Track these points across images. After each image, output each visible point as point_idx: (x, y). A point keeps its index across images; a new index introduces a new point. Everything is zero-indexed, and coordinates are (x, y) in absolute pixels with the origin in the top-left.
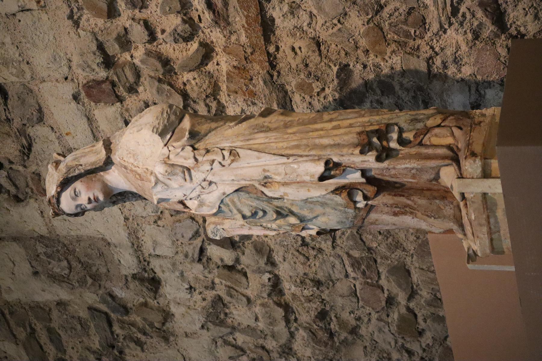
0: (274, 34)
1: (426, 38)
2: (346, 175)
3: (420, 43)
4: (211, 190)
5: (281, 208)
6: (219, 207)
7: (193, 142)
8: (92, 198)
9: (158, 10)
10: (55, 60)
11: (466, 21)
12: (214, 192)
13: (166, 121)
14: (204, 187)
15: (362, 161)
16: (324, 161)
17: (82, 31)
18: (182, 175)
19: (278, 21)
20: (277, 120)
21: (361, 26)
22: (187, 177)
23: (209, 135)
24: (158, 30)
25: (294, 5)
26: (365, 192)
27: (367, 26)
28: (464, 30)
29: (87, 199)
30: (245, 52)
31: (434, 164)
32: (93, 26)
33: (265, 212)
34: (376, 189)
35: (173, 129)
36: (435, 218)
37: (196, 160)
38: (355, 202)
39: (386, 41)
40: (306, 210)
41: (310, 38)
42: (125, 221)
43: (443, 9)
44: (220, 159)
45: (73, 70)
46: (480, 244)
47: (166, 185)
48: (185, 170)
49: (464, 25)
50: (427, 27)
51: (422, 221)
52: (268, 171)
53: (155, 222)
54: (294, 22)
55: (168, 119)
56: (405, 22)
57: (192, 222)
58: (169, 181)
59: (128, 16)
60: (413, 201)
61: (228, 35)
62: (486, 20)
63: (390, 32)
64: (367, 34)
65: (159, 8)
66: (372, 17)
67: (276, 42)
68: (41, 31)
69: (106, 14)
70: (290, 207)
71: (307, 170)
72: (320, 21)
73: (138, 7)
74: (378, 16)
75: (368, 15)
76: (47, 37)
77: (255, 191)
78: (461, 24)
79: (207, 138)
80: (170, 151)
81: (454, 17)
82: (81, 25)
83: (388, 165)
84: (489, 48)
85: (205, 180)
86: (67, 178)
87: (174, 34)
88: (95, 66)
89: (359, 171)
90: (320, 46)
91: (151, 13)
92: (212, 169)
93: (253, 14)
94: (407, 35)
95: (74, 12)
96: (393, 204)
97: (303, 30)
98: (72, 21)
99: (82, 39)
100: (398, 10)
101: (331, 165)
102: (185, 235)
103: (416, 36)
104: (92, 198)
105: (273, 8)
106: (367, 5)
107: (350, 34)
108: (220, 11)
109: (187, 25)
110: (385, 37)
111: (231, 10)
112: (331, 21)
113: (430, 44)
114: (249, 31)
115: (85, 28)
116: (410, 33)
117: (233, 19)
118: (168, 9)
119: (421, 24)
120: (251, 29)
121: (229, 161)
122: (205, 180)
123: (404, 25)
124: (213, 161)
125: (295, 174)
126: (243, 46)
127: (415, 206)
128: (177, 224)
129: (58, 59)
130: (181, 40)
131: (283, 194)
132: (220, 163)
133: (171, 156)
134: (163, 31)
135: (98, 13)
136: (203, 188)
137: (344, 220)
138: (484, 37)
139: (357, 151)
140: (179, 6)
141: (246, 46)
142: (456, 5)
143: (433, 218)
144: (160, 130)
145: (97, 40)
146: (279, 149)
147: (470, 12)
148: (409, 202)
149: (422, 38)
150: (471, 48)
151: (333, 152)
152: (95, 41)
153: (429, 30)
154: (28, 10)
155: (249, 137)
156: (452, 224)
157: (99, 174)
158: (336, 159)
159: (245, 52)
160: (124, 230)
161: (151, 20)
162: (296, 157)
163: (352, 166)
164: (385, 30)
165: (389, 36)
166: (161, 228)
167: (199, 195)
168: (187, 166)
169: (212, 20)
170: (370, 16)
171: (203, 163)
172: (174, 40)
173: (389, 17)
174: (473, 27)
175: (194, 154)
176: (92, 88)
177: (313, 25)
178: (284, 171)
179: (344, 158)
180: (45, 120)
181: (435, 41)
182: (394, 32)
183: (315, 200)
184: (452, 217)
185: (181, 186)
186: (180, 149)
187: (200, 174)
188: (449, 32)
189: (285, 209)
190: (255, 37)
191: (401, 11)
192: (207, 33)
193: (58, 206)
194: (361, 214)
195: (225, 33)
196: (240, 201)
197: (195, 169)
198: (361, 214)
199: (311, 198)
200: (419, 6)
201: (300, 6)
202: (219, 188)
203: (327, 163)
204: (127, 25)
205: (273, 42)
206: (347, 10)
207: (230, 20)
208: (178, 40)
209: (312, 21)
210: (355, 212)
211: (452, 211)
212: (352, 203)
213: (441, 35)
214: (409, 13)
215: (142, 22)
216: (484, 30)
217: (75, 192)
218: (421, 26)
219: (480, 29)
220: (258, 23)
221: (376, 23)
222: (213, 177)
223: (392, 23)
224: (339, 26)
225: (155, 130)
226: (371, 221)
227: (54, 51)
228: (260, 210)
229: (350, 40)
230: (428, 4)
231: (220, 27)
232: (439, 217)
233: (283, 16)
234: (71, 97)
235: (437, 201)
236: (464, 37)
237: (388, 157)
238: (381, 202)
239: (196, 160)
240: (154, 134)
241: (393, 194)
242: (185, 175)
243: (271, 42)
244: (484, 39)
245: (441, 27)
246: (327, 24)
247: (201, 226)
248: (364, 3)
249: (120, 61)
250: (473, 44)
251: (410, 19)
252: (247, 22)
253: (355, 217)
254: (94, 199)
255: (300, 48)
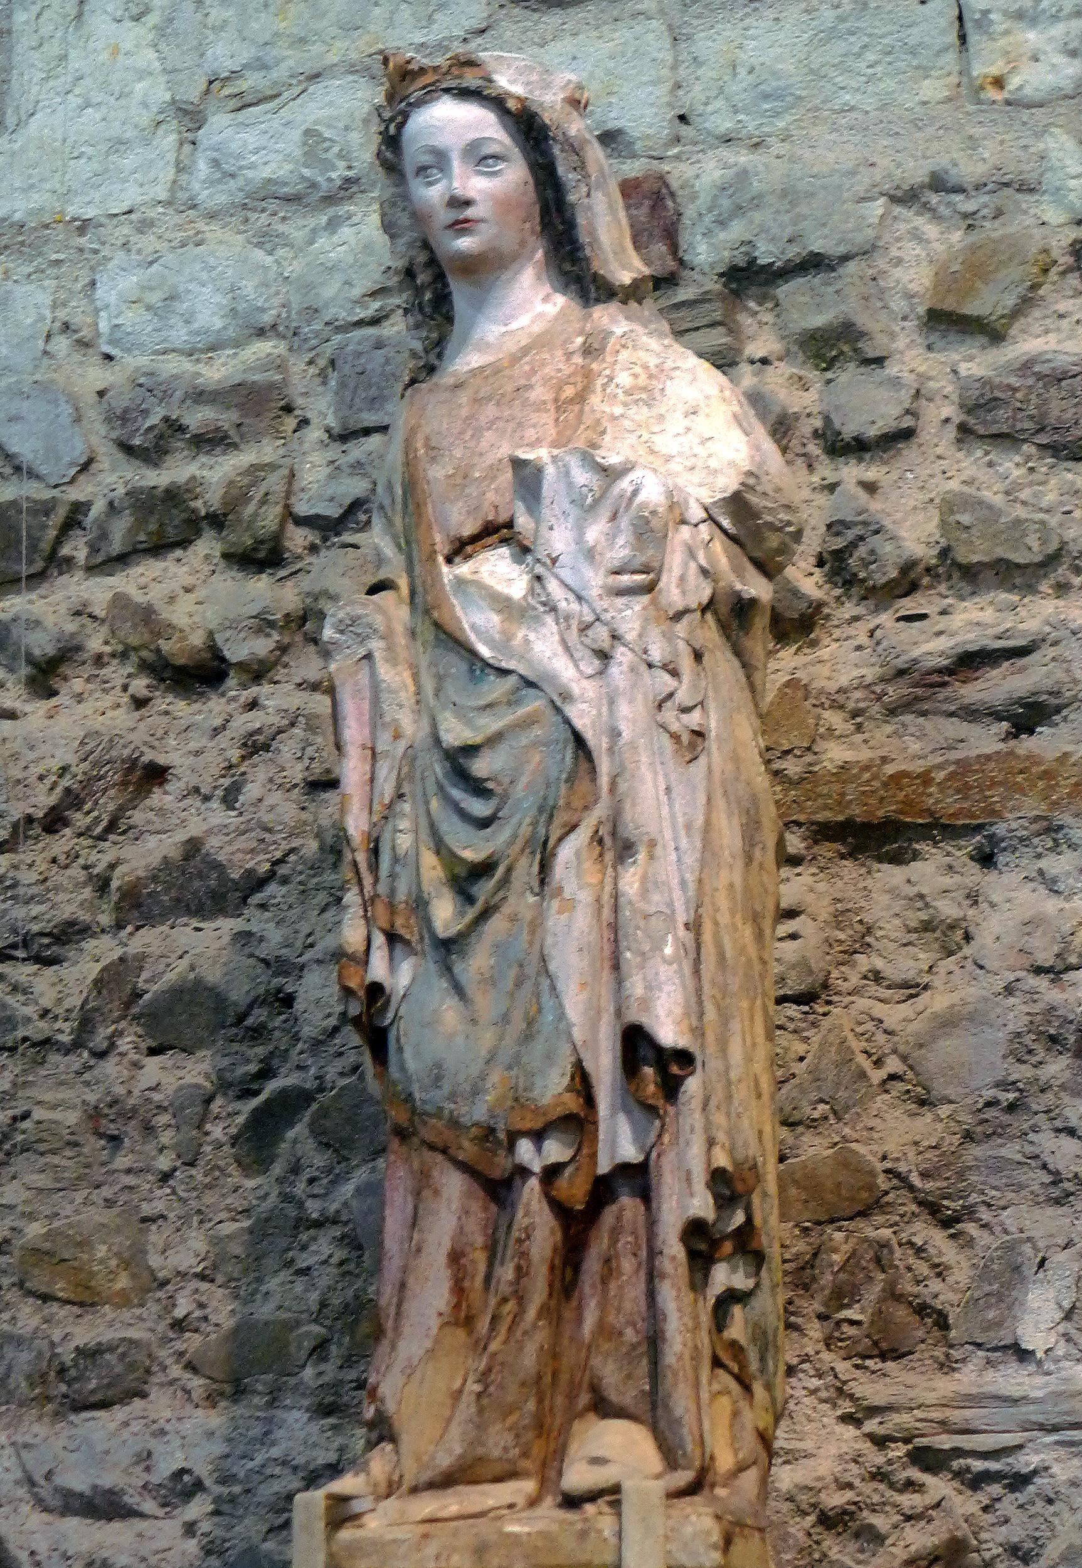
0: (843, 857)
1: (826, 1356)
2: (628, 1113)
3: (811, 1333)
4: (577, 655)
5: (505, 881)
6: (504, 672)
7: (724, 610)
8: (470, 213)
9: (954, 485)
10: (766, 97)
11: (889, 1493)
12: (571, 665)
13: (769, 518)
14: (590, 632)
15: (689, 1173)
16: (694, 1049)
17: (880, 211)
18: (637, 564)
19: (892, 875)
20: (766, 891)
21: (880, 1149)
22: (626, 579)
23: (736, 663)
24: (873, 473)
25: (959, 934)
26: (568, 1172)
27: (880, 1166)
28: (857, 1482)
29: (471, 194)
30: (787, 752)
31: (687, 1410)
32: (894, 252)
33: (484, 823)
34: (579, 1207)
35: (743, 539)
36: (479, 1395)
37: (678, 616)
38: (538, 1136)
39: (819, 1223)
40: (492, 962)
41: (829, 973)
42: (74, 220)
43: (942, 1423)
44: (683, 696)
45: (712, 147)
46: (394, 1541)
47: (596, 502)
48: (652, 576)
49: (875, 1485)
50: (869, 1363)
51: (428, 1344)
52: (651, 857)
53: (66, 327)
54: (891, 928)
55: (771, 526)
56: (893, 1295)
57: (71, 464)
58: (609, 514)
59: (930, 378)
60: (535, 1326)
61: (851, 705)
62: (895, 1556)
63: (852, 1241)
64: (846, 1161)
65: (966, 489)
66: (911, 1188)
67: (814, 858)
68: (879, 69)
69: (949, 304)
70: (506, 910)
71: (661, 990)
72: (895, 1014)
73: (972, 421)
74: (914, 1207)
75: (925, 1175)
76: (854, 84)
77: (577, 803)
78: (879, 1475)
79: (729, 655)
80: (696, 525)
81: (909, 1454)
82: (898, 210)
83: (674, 1258)
84: (788, 1557)
85: (615, 637)
86: (546, 138)
87: (865, 523)
88: (737, 230)
89: (641, 1158)
90: (799, 1003)
91: (939, 457)
92: (650, 666)
93: (938, 802)
94: (842, 1296)
95: (957, 198)
96: (529, 1262)
97: (855, 952)
98: (922, 186)
99: (849, 206)
100: (939, 1275)
101: (675, 1069)
102: (16, 428)
103: (838, 1323)
104: (470, 213)
105: (950, 867)
106: (961, 1175)
107: (847, 1109)
108: (943, 693)
109: (894, 574)
110: (832, 1221)
111: (954, 728)
112: (895, 1051)
113: (805, 1366)
114: (867, 776)
115: (889, 222)
116: (848, 1306)
117: (912, 730)
118: (965, 519)
119: (884, 1345)
120: (876, 784)
121: (675, 727)
122: (615, 637)
123: (883, 1290)
124: (675, 673)
125: (647, 947)
126: (809, 749)
127: (519, 1333)
128: (66, 410)
129: (766, 106)
130: (838, 543)
131: (567, 894)
132: (671, 695)
133: (685, 532)
134: (870, 488)
135: (946, 280)
136: (585, 628)
137: (446, 1088)
138: (826, 1544)
139: (721, 1160)
140: (975, 558)
141: (809, 758)
142: (956, 1464)
143: (477, 1388)
144: (748, 496)
145: (845, 258)
146: (713, 896)
147: (927, 1509)
148: (531, 1313)
149: (829, 1341)
150: (791, 1499)
151: (714, 1078)
152: (842, 250)
153: (857, 1367)
154: (963, 38)
155: (732, 798)
156: (458, 1450)
157: (539, 242)
158: (692, 1085)
159: (787, 752)
160: (41, 209)
161: (910, 453)
162: (692, 955)
163: (666, 1138)
164: (860, 1223)
165: (839, 1236)
166: (41, 343)
167: (554, 609)
168: (661, 585)
169: (915, 661)
170: (915, 1180)
171: (669, 637)
172: (841, 522)
173: (911, 1243)
174: (865, 1513)
175: (694, 611)
176: (653, 208)
177: (873, 989)
178: (653, 909)
179: (698, 1115)
180: (517, 11)
181: (815, 1383)
182: (854, 1253)
183: (547, 1001)
184: (480, 1451)
185: (590, 554)
186: (703, 563)
187: (637, 625)
188: (850, 1431)
189: (501, 894)
190: (843, 795)
191: (935, 1285)
192: (850, 631)
193: (447, 91)
194: (466, 1144)
195: (858, 694)
196: (535, 744)
197: (652, 612)
198: (466, 1144)
199: (553, 988)
200: (951, 1346)
201: (950, 954)
202: (585, 683)
203: (685, 1058)
204: (892, 369)
205: (816, 849)
206: (944, 1111)
207: (908, 718)
208: (838, 534)
209: (889, 987)
210: (476, 1124)
211: (496, 1453)
212: (538, 1124)
213: (835, 1406)
214: (922, 1310)
215: (907, 422)
216: (853, 1546)
217: (495, 157)
218: (876, 1343)
219: (857, 1535)
220: (901, 812)
221: (886, 1199)
222: (625, 668)
223: (892, 1252)
224: (877, 1076)
225: (751, 481)
226: (435, 1173)
227: (800, 98)
228: (498, 810)
229: (822, 1107)
230: (957, 1375)
231: (882, 680)
232: (481, 1411)
233: (921, 896)
234: (610, 125)
235: (531, 1405)
236: (830, 1479)
237: (693, 1255)
238: (537, 1220)
239: (678, 616)
240: (741, 479)
241: (557, 1262)
242: (634, 572)
243: (816, 842)
244: (818, 1543)
245: (874, 1411)
246: (881, 1038)
247: (55, 492)
248: (970, 1168)
249: (746, 321)
250: (804, 1506)
251: (901, 1313)
252: (904, 774)
253: (454, 1123)
254: (466, 221)
255: (793, 936)
